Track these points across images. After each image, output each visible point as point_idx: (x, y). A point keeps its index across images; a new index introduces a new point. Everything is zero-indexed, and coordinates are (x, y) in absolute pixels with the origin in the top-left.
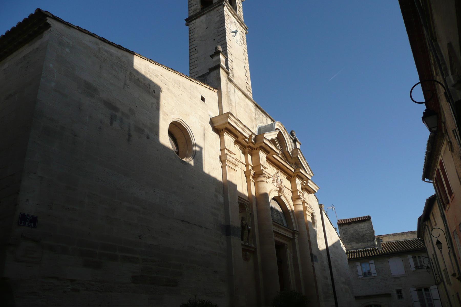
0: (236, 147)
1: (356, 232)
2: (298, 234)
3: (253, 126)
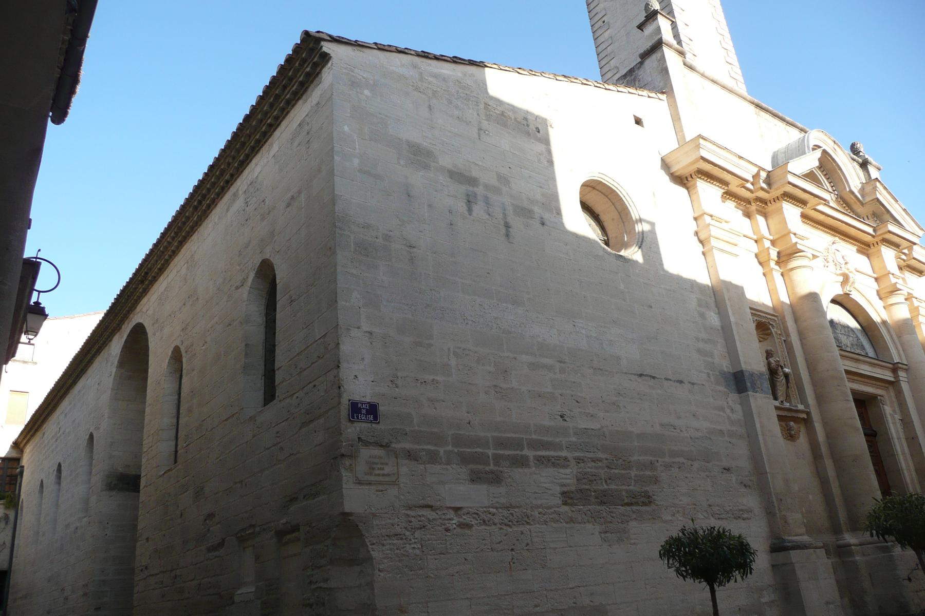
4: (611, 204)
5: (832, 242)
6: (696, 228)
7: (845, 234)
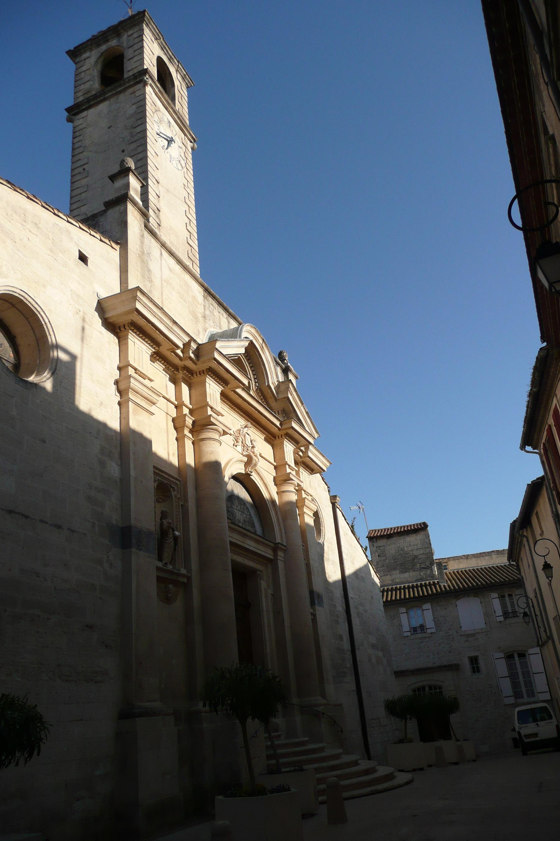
0: (156, 366)
1: (401, 552)
2: (285, 551)
3: (198, 329)
4: (31, 328)
5: (245, 425)
6: (118, 377)
7: (257, 421)
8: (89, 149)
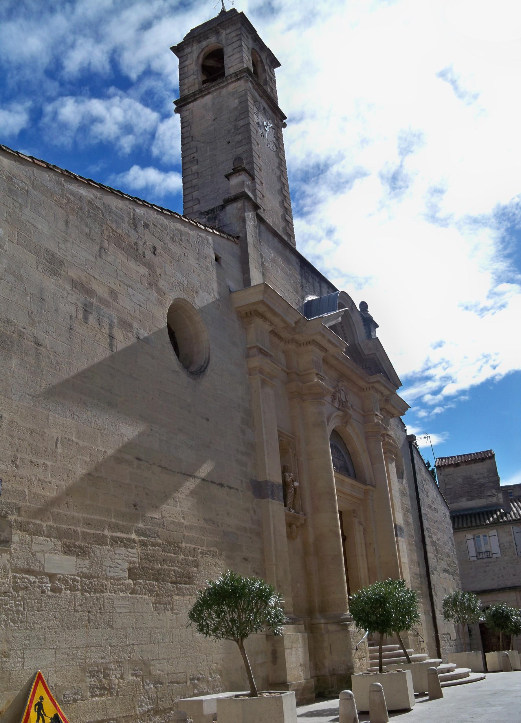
8: (197, 139)
